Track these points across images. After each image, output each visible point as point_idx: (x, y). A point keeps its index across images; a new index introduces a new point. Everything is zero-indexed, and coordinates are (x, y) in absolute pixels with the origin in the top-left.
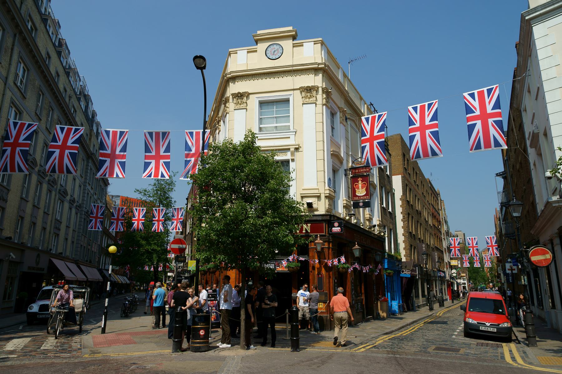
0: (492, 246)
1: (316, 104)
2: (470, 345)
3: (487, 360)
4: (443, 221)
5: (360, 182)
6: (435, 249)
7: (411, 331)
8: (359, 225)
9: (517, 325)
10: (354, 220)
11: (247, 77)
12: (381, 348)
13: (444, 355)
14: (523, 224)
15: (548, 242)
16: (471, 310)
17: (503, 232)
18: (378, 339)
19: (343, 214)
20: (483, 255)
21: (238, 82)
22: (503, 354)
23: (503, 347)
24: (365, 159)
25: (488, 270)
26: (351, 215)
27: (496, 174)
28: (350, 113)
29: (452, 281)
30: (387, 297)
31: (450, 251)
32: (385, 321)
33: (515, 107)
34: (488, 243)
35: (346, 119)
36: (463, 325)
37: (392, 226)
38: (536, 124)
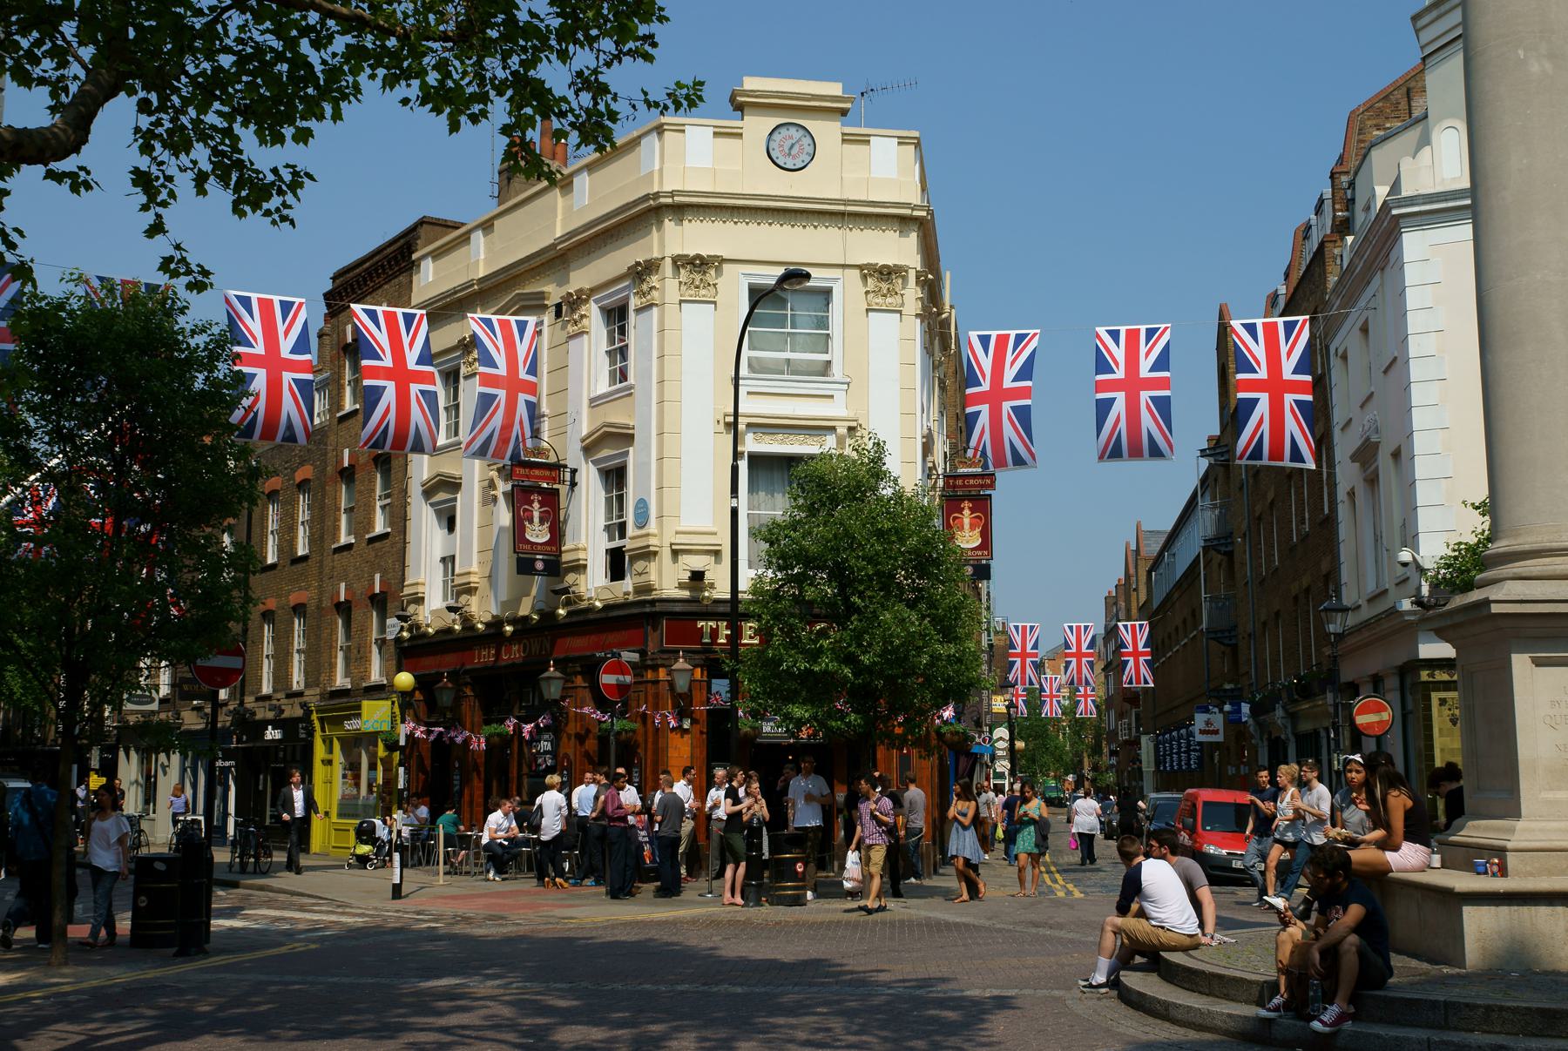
5: (967, 512)
11: (718, 210)
21: (690, 221)
24: (976, 449)
27: (1201, 451)
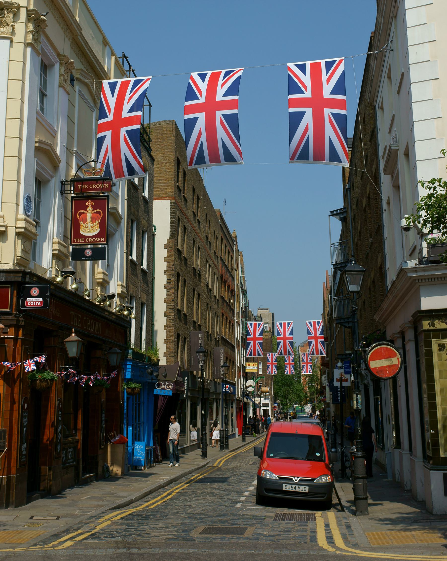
0: (316, 338)
1: (12, 42)
2: (264, 519)
3: (287, 544)
4: (238, 289)
5: (90, 209)
6: (220, 342)
7: (166, 499)
8: (82, 295)
9: (343, 477)
10: (72, 284)
12: (105, 537)
13: (219, 541)
14: (364, 302)
15: (398, 336)
16: (272, 455)
17: (334, 315)
18: (102, 520)
19: (51, 271)
20: (301, 353)
22: (314, 531)
23: (315, 520)
24: (103, 164)
25: (307, 380)
26: (66, 274)
27: (331, 212)
28: (81, 70)
29: (245, 400)
30: (125, 435)
31: (246, 345)
32: (117, 482)
33: (367, 100)
34: (309, 333)
35: (72, 80)
36: (255, 483)
37: (145, 296)
38: (396, 135)
